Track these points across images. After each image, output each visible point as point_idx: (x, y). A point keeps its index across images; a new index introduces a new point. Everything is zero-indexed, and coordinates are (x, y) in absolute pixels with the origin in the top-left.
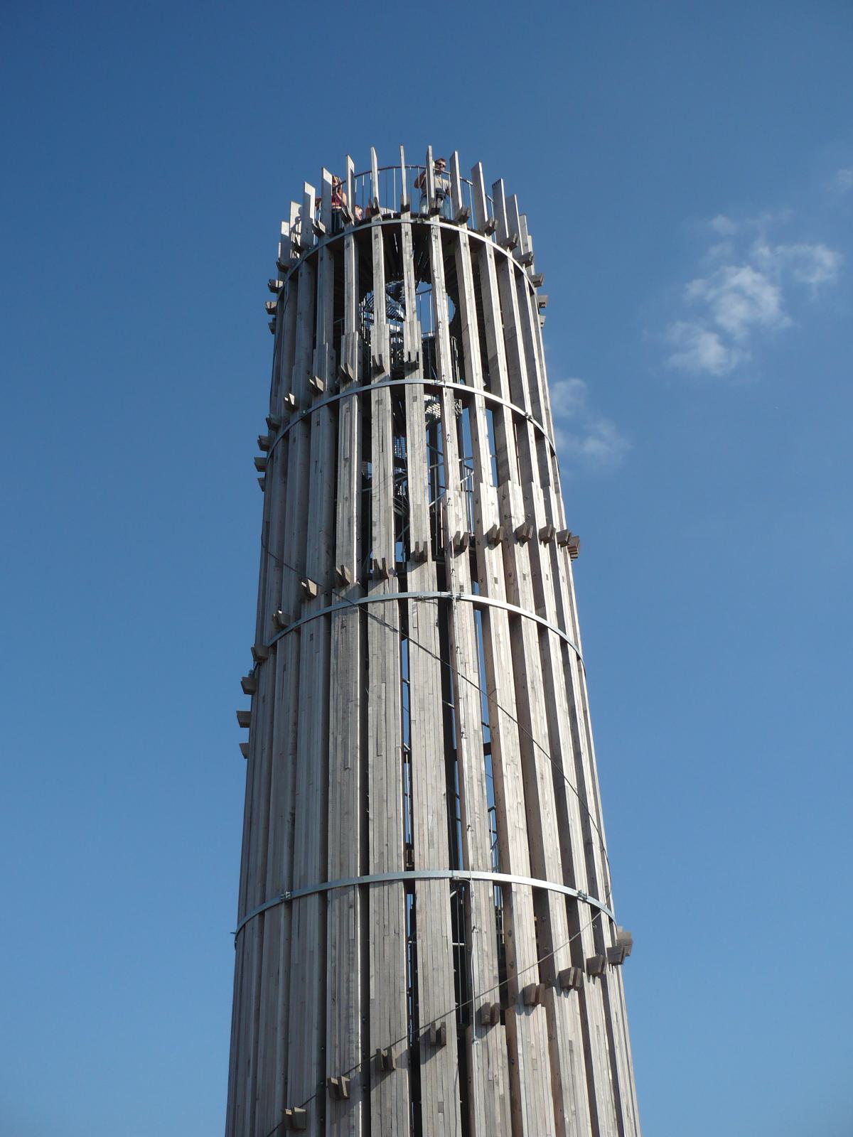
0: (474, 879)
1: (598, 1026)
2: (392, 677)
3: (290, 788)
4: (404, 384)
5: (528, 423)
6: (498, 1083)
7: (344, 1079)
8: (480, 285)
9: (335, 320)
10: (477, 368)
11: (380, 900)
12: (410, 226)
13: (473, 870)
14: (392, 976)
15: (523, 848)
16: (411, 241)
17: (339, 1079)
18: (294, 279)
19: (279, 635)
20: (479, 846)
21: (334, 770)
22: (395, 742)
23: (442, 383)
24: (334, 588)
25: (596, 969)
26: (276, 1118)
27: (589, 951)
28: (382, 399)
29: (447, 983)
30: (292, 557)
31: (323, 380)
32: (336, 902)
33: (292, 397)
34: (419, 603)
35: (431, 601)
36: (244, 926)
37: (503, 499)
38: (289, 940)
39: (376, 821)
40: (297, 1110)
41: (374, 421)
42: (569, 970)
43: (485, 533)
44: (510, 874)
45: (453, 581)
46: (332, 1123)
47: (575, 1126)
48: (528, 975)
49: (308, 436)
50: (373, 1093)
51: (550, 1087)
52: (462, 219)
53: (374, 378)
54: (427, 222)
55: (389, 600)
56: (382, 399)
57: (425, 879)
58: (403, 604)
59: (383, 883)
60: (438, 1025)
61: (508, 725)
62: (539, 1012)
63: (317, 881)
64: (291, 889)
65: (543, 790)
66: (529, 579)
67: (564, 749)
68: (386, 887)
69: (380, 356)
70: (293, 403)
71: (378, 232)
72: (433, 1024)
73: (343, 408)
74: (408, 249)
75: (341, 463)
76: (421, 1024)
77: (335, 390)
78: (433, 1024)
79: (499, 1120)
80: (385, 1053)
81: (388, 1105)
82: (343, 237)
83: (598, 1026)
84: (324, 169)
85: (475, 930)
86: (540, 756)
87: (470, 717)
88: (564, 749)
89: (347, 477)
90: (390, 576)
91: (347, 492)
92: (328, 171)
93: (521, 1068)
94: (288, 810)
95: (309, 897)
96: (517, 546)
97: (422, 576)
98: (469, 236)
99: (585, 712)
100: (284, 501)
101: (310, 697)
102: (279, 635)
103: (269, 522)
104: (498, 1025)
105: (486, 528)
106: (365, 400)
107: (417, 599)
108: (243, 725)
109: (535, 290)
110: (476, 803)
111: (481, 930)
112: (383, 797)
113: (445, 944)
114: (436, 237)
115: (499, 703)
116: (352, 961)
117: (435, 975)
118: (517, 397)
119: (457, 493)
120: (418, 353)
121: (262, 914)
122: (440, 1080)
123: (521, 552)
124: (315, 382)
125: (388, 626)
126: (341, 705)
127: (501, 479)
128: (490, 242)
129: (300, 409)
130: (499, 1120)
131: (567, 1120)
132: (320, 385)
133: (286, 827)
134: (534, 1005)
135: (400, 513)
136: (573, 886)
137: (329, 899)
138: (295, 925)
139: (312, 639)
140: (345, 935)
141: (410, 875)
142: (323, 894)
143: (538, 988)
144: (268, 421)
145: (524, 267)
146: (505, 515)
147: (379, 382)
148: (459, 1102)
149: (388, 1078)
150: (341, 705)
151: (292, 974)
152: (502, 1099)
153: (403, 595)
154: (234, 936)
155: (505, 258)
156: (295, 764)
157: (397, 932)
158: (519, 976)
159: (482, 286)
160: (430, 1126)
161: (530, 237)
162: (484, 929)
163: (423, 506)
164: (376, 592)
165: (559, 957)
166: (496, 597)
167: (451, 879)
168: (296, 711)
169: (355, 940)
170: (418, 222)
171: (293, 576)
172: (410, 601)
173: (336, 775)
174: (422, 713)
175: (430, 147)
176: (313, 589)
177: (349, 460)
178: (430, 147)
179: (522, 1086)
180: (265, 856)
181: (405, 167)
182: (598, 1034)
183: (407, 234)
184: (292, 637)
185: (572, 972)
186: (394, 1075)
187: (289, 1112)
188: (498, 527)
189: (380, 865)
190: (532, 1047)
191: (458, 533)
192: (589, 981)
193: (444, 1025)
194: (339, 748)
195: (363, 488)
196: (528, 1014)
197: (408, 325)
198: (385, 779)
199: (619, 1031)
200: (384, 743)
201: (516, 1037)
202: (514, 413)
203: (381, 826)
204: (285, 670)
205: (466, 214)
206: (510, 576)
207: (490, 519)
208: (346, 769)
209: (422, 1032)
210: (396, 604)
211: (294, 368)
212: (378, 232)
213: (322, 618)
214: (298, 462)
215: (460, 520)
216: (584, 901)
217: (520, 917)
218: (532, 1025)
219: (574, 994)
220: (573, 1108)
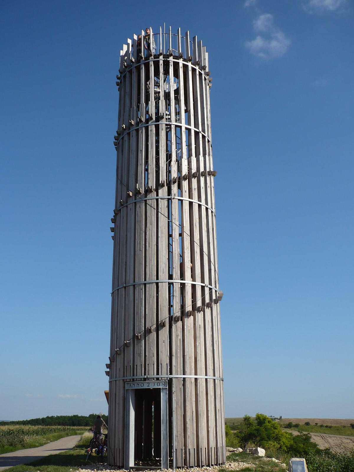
0: (174, 378)
1: (208, 321)
2: (153, 223)
3: (125, 255)
4: (159, 124)
5: (200, 133)
7: (139, 334)
9: (138, 96)
11: (149, 288)
12: (162, 61)
13: (175, 280)
14: (152, 308)
15: (189, 274)
17: (138, 334)
18: (125, 77)
19: (121, 207)
20: (177, 273)
21: (137, 251)
22: (153, 230)
23: (171, 123)
24: (137, 194)
25: (209, 305)
26: (122, 344)
27: (207, 300)
28: (152, 129)
29: (166, 310)
30: (125, 182)
31: (134, 121)
32: (138, 288)
33: (124, 126)
34: (162, 200)
35: (166, 199)
36: (113, 292)
38: (125, 297)
39: (148, 266)
40: (127, 342)
41: (149, 137)
43: (183, 176)
44: (185, 280)
46: (136, 345)
47: (199, 346)
49: (129, 139)
50: (147, 338)
51: (193, 336)
53: (150, 121)
54: (168, 59)
55: (153, 199)
56: (152, 129)
57: (161, 282)
58: (157, 200)
59: (150, 283)
60: (163, 321)
61: (187, 237)
62: (191, 318)
63: (133, 282)
64: (125, 284)
65: (196, 255)
66: (197, 190)
67: (204, 243)
68: (151, 284)
69: (151, 114)
70: (124, 128)
71: (152, 63)
72: (162, 321)
73: (140, 131)
74: (161, 71)
75: (139, 152)
76: (159, 321)
77: (137, 124)
78: (162, 321)
79: (179, 345)
80: (149, 328)
81: (150, 341)
82: (140, 65)
83: (208, 321)
84: (134, 34)
86: (196, 246)
87: (176, 235)
88: (204, 243)
89: (141, 157)
90: (154, 191)
91: (141, 162)
92: (135, 34)
93: (185, 332)
94: (125, 261)
95: (130, 286)
96: (193, 179)
97: (163, 191)
98: (183, 63)
99: (213, 229)
100: (122, 159)
101: (130, 228)
102: (121, 207)
105: (183, 174)
106: (147, 128)
107: (161, 199)
110: (176, 261)
112: (150, 259)
115: (184, 231)
116: (142, 304)
118: (196, 125)
119: (174, 163)
121: (118, 290)
122: (164, 335)
123: (202, 179)
124: (131, 121)
125: (153, 207)
126: (139, 231)
128: (190, 64)
129: (127, 130)
130: (179, 345)
131: (197, 345)
132: (133, 122)
133: (124, 266)
134: (190, 316)
135: (157, 170)
136: (204, 283)
137: (136, 287)
138: (127, 294)
139: (131, 210)
140: (140, 297)
141: (157, 281)
142: (134, 285)
143: (191, 311)
144: (117, 132)
145: (203, 71)
146: (190, 169)
147: (152, 123)
148: (169, 340)
149: (151, 334)
150: (139, 231)
151: (126, 307)
152: (180, 339)
153: (157, 197)
154: (111, 294)
155: (195, 69)
156: (126, 247)
160: (161, 346)
162: (177, 296)
164: (149, 196)
165: (198, 302)
166: (186, 198)
167: (168, 282)
168: (127, 232)
169: (142, 298)
171: (125, 188)
173: (137, 252)
174: (162, 234)
175: (170, 27)
176: (131, 194)
177: (142, 151)
178: (170, 27)
179: (185, 336)
180: (119, 273)
181: (162, 34)
182: (208, 323)
183: (161, 65)
184: (125, 208)
185: (201, 307)
186: (152, 333)
187: (125, 342)
189: (149, 278)
190: (189, 326)
191: (174, 177)
192: (207, 309)
193: (165, 321)
194: (138, 244)
195: (146, 93)
196: (188, 318)
197: (161, 101)
198: (151, 254)
199: (215, 321)
200: (151, 243)
203: (150, 267)
204: (123, 218)
205: (182, 55)
208: (140, 251)
209: (159, 323)
212: (152, 63)
213: (134, 203)
214: (126, 149)
215: (175, 172)
216: (207, 287)
217: (187, 292)
218: (189, 321)
219: (202, 312)
220: (199, 342)
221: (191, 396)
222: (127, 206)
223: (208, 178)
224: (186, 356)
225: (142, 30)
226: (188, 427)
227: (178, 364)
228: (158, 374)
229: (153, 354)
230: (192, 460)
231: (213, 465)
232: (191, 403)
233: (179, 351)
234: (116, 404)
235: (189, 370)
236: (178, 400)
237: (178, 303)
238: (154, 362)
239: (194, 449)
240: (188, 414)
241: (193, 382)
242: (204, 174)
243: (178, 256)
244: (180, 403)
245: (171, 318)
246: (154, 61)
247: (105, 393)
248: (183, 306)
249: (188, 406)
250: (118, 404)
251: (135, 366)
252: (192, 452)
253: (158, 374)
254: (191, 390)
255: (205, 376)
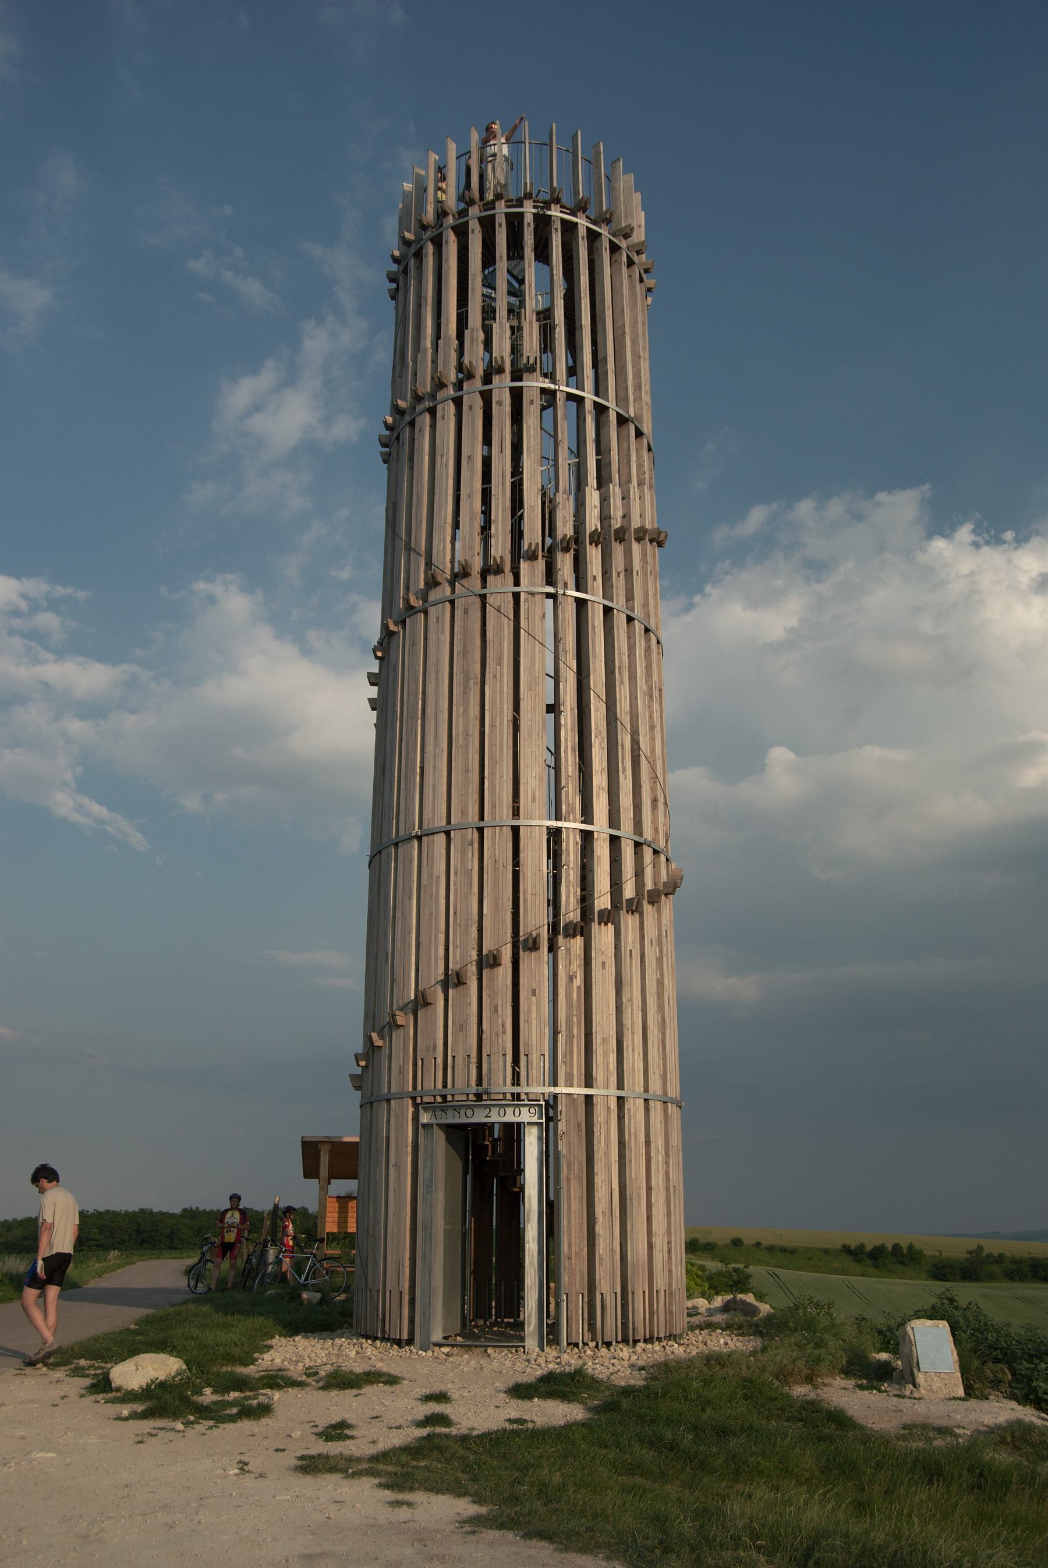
6: (576, 977)
16: (533, 234)
21: (457, 736)
23: (557, 387)
25: (606, 917)
28: (473, 403)
36: (380, 852)
37: (604, 500)
42: (633, 898)
45: (559, 578)
48: (602, 901)
51: (614, 982)
52: (580, 207)
54: (549, 213)
56: (473, 403)
69: (502, 357)
71: (474, 226)
74: (529, 241)
76: (521, 933)
83: (651, 940)
86: (622, 730)
95: (435, 836)
103: (396, 503)
104: (578, 937)
106: (458, 402)
108: (372, 684)
111: (569, 867)
113: (541, 875)
123: (618, 550)
136: (641, 834)
146: (605, 517)
152: (579, 988)
153: (517, 589)
159: (596, 281)
161: (639, 195)
162: (571, 865)
170: (541, 213)
172: (522, 595)
175: (554, 125)
183: (529, 224)
185: (636, 901)
188: (599, 530)
193: (538, 935)
201: (591, 945)
205: (585, 205)
206: (606, 573)
207: (593, 522)
209: (521, 939)
210: (510, 596)
212: (474, 226)
217: (599, 858)
221: (608, 1145)
224: (594, 1035)
227: (573, 1057)
228: (516, 1080)
229: (503, 1025)
230: (611, 1324)
231: (661, 1338)
232: (609, 1167)
233: (575, 1019)
236: (572, 1157)
239: (616, 1293)
241: (612, 1108)
242: (621, 536)
243: (573, 756)
244: (579, 1165)
245: (554, 928)
247: (303, 1142)
248: (586, 899)
250: (395, 1165)
251: (420, 1062)
253: (516, 1080)
254: (608, 1131)
255: (618, 1089)
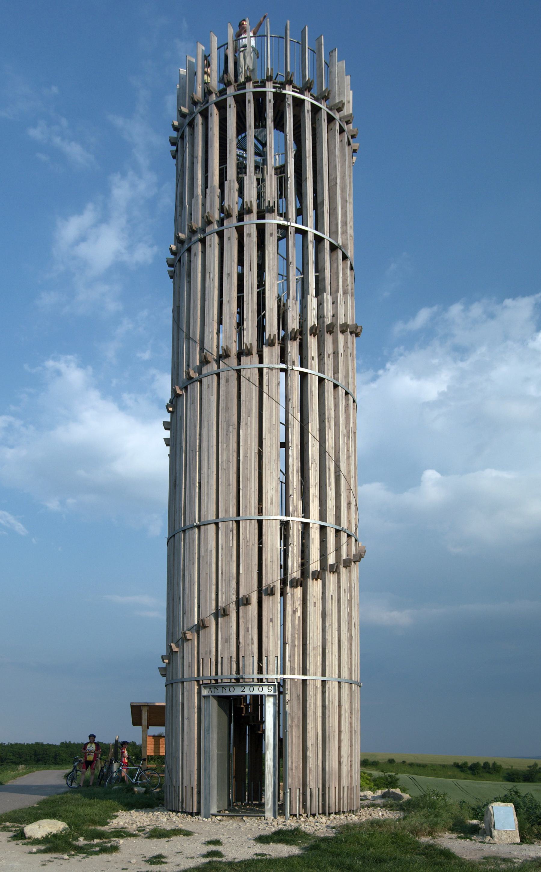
6: (297, 611)
8: (316, 143)
10: (311, 203)
12: (272, 93)
13: (291, 516)
21: (222, 462)
23: (289, 224)
25: (335, 569)
36: (174, 536)
37: (320, 304)
42: (334, 564)
45: (289, 359)
48: (314, 565)
54: (284, 92)
60: (272, 586)
71: (231, 102)
74: (270, 114)
76: (264, 585)
85: (291, 545)
104: (299, 587)
109: (351, 141)
111: (293, 545)
113: (276, 550)
114: (289, 105)
117: (271, 564)
119: (294, 302)
120: (274, 202)
127: (319, 292)
146: (320, 316)
152: (299, 617)
157: (253, 544)
158: (310, 566)
163: (274, 310)
172: (264, 370)
175: (288, 22)
183: (270, 101)
185: (336, 565)
191: (294, 329)
193: (274, 586)
202: (331, 243)
206: (321, 354)
207: (312, 320)
210: (257, 370)
211: (193, 200)
212: (231, 102)
217: (313, 539)
221: (316, 708)
222: (201, 382)
223: (341, 337)
224: (308, 645)
225: (229, 24)
226: (309, 757)
228: (260, 671)
229: (252, 639)
230: (315, 804)
233: (297, 636)
234: (185, 719)
235: (313, 667)
237: (297, 556)
238: (253, 654)
239: (319, 788)
240: (311, 735)
242: (331, 329)
243: (297, 475)
245: (284, 582)
246: (234, 96)
249: (310, 723)
250: (187, 719)
252: (315, 792)
253: (260, 671)
254: (316, 700)
